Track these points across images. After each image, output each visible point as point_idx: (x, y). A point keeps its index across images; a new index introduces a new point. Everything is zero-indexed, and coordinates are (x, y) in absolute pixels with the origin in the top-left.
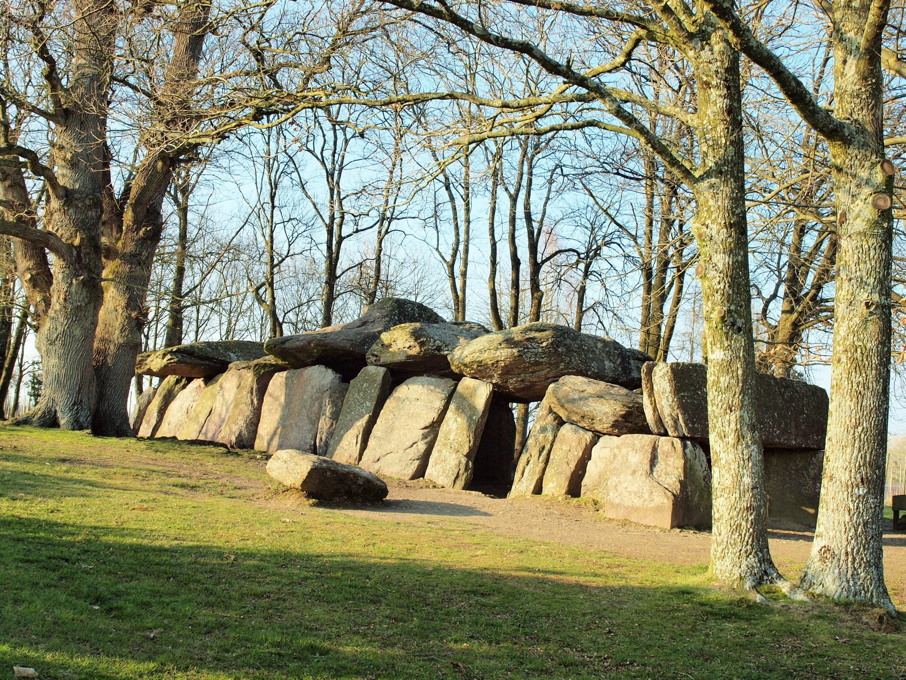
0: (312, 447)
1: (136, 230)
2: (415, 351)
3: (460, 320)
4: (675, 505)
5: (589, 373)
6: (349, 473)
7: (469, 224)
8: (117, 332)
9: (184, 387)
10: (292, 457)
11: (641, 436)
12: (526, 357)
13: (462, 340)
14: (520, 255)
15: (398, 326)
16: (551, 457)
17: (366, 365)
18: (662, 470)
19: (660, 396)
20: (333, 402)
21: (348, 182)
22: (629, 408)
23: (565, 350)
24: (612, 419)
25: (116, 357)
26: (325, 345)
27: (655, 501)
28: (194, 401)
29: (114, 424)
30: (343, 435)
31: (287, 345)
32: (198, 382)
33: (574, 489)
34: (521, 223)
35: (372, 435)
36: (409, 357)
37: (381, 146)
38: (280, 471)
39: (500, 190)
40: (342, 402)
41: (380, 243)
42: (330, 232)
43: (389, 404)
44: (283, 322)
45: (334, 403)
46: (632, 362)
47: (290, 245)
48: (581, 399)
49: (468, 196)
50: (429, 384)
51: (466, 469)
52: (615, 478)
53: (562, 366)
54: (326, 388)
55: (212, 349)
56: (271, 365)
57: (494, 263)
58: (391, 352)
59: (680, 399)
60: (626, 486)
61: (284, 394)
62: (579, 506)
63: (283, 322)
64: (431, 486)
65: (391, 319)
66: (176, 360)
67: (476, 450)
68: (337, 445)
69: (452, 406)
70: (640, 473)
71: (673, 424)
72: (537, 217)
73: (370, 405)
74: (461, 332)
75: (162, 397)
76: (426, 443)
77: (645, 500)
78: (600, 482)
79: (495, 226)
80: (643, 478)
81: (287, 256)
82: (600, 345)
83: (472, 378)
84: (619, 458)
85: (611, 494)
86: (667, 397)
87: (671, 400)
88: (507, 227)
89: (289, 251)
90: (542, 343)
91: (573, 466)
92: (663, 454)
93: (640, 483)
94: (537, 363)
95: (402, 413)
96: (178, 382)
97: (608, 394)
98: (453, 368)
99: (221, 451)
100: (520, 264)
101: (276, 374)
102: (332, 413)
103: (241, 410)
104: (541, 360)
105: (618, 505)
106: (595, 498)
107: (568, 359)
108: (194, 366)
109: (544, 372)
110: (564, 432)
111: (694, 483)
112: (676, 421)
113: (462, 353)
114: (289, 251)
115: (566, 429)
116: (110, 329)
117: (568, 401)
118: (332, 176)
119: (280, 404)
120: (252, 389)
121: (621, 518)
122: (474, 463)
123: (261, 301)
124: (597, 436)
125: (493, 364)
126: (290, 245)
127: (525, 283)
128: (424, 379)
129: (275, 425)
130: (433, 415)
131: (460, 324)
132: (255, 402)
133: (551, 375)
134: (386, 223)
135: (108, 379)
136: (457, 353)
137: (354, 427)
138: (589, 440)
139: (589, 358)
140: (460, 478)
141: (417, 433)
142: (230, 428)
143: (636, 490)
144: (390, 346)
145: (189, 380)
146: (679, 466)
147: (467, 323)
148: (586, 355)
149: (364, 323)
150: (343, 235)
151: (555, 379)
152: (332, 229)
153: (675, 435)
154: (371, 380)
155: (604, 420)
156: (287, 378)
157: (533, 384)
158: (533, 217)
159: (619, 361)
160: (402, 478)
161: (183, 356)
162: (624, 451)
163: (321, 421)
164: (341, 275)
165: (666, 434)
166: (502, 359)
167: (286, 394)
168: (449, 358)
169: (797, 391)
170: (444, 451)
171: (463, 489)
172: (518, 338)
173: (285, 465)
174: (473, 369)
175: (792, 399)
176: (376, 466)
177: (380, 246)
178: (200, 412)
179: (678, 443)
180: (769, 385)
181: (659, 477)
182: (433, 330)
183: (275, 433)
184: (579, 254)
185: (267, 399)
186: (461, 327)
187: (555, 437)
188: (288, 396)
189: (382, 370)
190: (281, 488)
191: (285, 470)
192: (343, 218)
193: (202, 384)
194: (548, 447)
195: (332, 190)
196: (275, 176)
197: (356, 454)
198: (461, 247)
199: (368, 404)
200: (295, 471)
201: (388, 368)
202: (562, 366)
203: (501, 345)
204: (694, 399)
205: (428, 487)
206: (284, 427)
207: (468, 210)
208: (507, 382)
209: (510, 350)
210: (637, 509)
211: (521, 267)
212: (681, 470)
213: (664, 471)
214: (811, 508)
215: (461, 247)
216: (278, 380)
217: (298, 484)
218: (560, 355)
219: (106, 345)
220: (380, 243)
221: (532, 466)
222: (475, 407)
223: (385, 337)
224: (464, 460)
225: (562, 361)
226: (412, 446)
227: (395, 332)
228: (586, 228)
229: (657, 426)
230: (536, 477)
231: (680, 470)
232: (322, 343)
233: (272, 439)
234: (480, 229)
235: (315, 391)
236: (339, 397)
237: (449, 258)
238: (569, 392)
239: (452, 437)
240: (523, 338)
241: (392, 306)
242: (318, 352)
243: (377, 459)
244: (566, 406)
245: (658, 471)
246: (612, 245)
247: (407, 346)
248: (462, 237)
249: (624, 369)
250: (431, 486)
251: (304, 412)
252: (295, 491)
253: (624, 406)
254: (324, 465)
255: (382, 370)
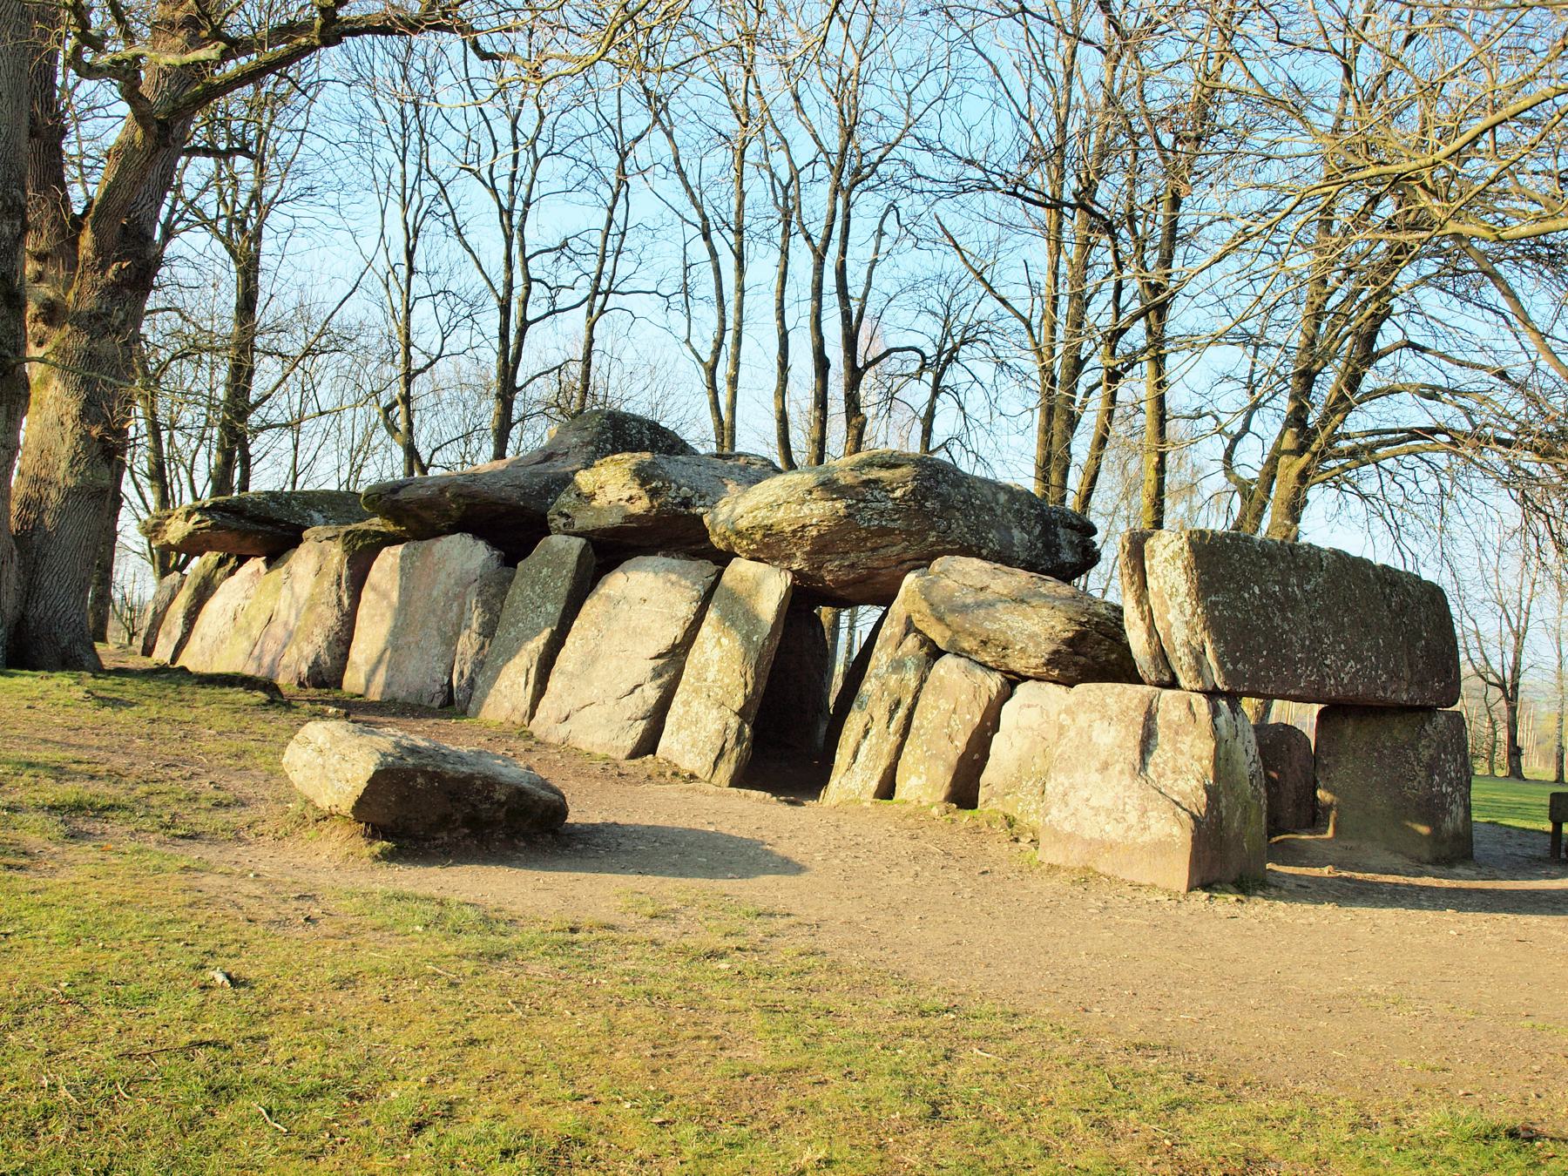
0: (446, 688)
1: (100, 267)
2: (641, 506)
3: (726, 450)
4: (1197, 840)
5: (984, 552)
6: (471, 777)
7: (743, 295)
8: (64, 465)
9: (232, 572)
10: (335, 741)
11: (1118, 687)
12: (862, 518)
13: (731, 486)
14: (828, 352)
15: (608, 459)
16: (915, 723)
17: (549, 533)
18: (1165, 763)
19: (1163, 603)
20: (485, 603)
21: (541, 229)
22: (1081, 624)
23: (938, 506)
24: (1047, 648)
25: (61, 513)
26: (472, 496)
27: (1153, 830)
28: (247, 598)
29: (58, 644)
30: (501, 667)
31: (402, 495)
32: (256, 564)
33: (964, 792)
34: (831, 302)
35: (555, 668)
36: (630, 518)
37: (595, 168)
38: (308, 773)
39: (798, 241)
40: (502, 603)
41: (591, 329)
42: (505, 310)
43: (592, 608)
44: (430, 464)
45: (487, 606)
46: (1061, 531)
47: (444, 339)
48: (979, 605)
49: (741, 245)
50: (668, 571)
51: (739, 741)
52: (1062, 778)
53: (932, 537)
54: (474, 577)
55: (280, 504)
56: (378, 533)
57: (784, 366)
58: (594, 508)
59: (1210, 609)
60: (1086, 796)
61: (397, 588)
62: (976, 830)
63: (430, 464)
64: (668, 774)
65: (598, 448)
66: (210, 523)
67: (758, 701)
68: (490, 686)
69: (712, 615)
70: (1118, 767)
71: (1193, 663)
72: (855, 290)
73: (553, 609)
74: (731, 472)
75: (192, 590)
76: (659, 687)
77: (1130, 828)
78: (1020, 779)
79: (786, 305)
80: (1127, 780)
81: (439, 357)
82: (1003, 497)
83: (752, 559)
84: (1072, 734)
85: (1054, 811)
86: (1181, 605)
87: (1188, 611)
88: (807, 307)
89: (442, 349)
90: (893, 491)
91: (961, 743)
92: (1169, 727)
93: (1120, 789)
94: (883, 532)
95: (615, 626)
96: (221, 563)
97: (1035, 595)
98: (714, 539)
99: (254, 700)
100: (829, 366)
101: (385, 549)
102: (483, 625)
103: (320, 616)
104: (892, 525)
105: (1070, 836)
106: (1008, 811)
107: (943, 525)
108: (245, 534)
109: (896, 549)
110: (942, 672)
111: (1232, 789)
112: (1198, 656)
113: (733, 510)
114: (442, 349)
115: (947, 667)
116: (51, 460)
117: (953, 611)
118: (511, 224)
119: (390, 605)
120: (340, 577)
121: (1074, 864)
122: (754, 728)
123: (392, 429)
124: (1013, 680)
125: (794, 532)
126: (444, 339)
127: (837, 406)
128: (658, 560)
129: (381, 645)
130: (675, 632)
131: (729, 457)
132: (346, 601)
133: (910, 554)
134: (600, 299)
135: (45, 555)
136: (723, 511)
137: (523, 652)
138: (995, 691)
139: (985, 523)
140: (726, 757)
141: (643, 667)
142: (299, 649)
143: (1109, 805)
144: (592, 497)
145: (242, 560)
146: (1205, 754)
147: (740, 455)
148: (977, 517)
149: (548, 456)
150: (529, 318)
151: (923, 561)
152: (509, 303)
153: (1197, 687)
154: (556, 562)
155: (1031, 649)
156: (403, 558)
157: (873, 572)
158: (850, 292)
159: (1037, 531)
160: (611, 754)
161: (222, 516)
162: (1082, 719)
163: (463, 639)
164: (524, 386)
165: (1173, 684)
166: (814, 521)
167: (400, 586)
168: (706, 520)
169: (1409, 594)
170: (695, 704)
171: (731, 785)
172: (846, 479)
173: (320, 760)
174: (753, 541)
175: (1403, 608)
176: (563, 730)
177: (591, 335)
178: (254, 618)
179: (1201, 704)
180: (1366, 580)
181: (1159, 776)
182: (674, 467)
183: (379, 661)
184: (924, 357)
185: (367, 594)
186: (730, 463)
187: (923, 681)
188: (405, 591)
189: (578, 543)
190: (311, 815)
191: (319, 770)
192: (528, 289)
193: (263, 567)
194: (907, 701)
195: (509, 240)
196: (416, 218)
197: (525, 705)
198: (729, 337)
199: (550, 608)
200: (340, 775)
201: (588, 539)
202: (932, 537)
203: (810, 493)
204: (1235, 608)
205: (662, 774)
206: (396, 649)
207: (741, 270)
208: (820, 568)
209: (830, 503)
210: (1111, 847)
211: (831, 372)
212: (1207, 764)
213: (1170, 765)
214: (1425, 825)
215: (729, 337)
216: (388, 561)
217: (346, 806)
218: (928, 515)
219: (42, 490)
220: (591, 329)
221: (874, 741)
222: (756, 617)
223: (584, 479)
224: (734, 722)
225: (932, 528)
226: (632, 692)
227: (602, 470)
228: (935, 314)
229: (1156, 666)
230: (884, 763)
231: (1206, 762)
232: (465, 491)
233: (373, 671)
234: (760, 306)
235: (453, 581)
236: (495, 593)
237: (707, 357)
238: (954, 590)
239: (710, 675)
240: (856, 481)
241: (601, 425)
242: (459, 508)
243: (564, 715)
244: (948, 619)
245: (1156, 765)
246: (977, 344)
247: (626, 495)
248: (730, 324)
249: (1047, 545)
250: (668, 774)
251: (433, 622)
252: (339, 823)
253: (1070, 619)
254: (410, 761)
255: (578, 543)
